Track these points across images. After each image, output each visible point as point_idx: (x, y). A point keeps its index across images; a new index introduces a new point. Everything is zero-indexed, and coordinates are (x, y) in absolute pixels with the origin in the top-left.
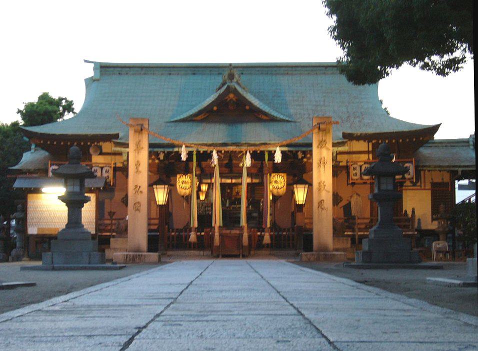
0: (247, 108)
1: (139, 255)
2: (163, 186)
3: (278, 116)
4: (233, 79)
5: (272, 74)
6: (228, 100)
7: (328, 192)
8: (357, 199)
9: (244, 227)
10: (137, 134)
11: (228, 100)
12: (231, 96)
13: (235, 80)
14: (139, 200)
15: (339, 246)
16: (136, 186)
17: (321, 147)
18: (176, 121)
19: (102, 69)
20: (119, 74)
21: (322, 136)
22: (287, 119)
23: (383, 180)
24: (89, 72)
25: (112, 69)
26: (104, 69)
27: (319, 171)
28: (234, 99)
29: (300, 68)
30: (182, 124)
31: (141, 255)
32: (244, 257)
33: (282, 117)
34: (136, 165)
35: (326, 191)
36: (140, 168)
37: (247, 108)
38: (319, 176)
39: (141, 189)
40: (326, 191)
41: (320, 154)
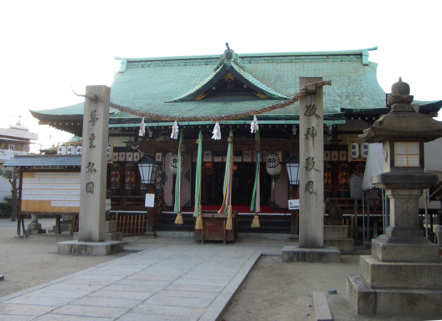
0: (245, 86)
1: (85, 246)
2: (148, 165)
3: (276, 94)
4: (231, 59)
5: (277, 63)
6: (226, 79)
7: (318, 171)
8: (356, 179)
9: (195, 218)
10: (93, 103)
11: (226, 79)
12: (229, 76)
13: (232, 60)
14: (91, 180)
15: (334, 236)
16: (90, 163)
17: (310, 115)
18: (175, 101)
19: (128, 64)
20: (142, 66)
21: (311, 101)
22: (285, 97)
23: (400, 148)
24: (118, 67)
25: (137, 63)
26: (131, 63)
27: (307, 145)
28: (232, 79)
29: (303, 57)
30: (179, 104)
31: (88, 246)
32: (229, 242)
33: (279, 95)
34: (90, 139)
35: (316, 170)
36: (95, 143)
37: (245, 86)
38: (307, 150)
39: (94, 167)
40: (316, 170)
41: (309, 122)
